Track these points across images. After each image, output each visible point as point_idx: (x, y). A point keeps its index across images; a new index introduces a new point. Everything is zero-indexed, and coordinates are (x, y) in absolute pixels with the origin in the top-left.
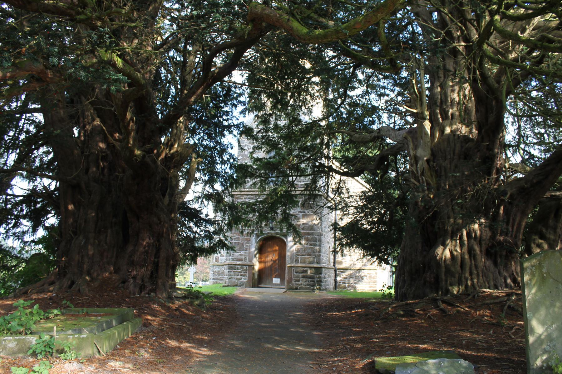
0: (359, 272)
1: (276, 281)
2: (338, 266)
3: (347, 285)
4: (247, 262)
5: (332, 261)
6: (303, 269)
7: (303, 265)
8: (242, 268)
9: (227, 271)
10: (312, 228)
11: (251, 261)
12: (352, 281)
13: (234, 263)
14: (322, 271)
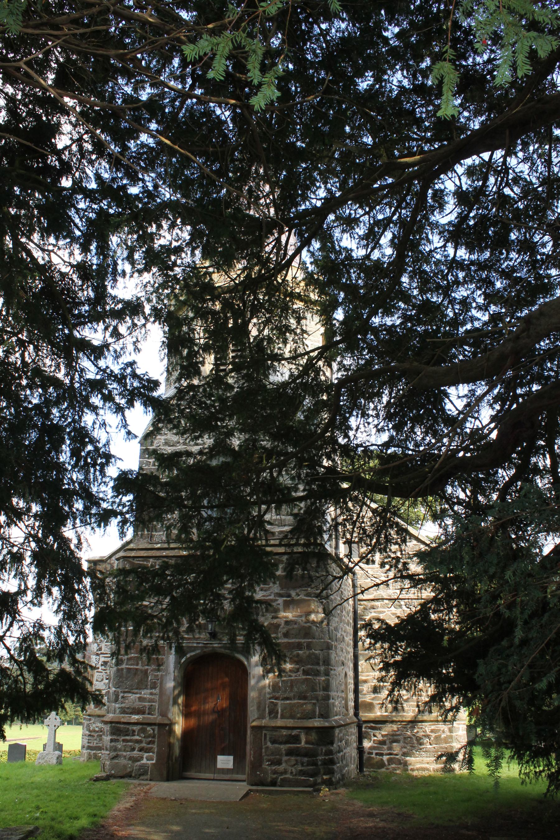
0: (413, 728)
1: (225, 761)
2: (365, 715)
3: (385, 758)
4: (156, 717)
5: (352, 704)
6: (289, 732)
7: (290, 723)
8: (143, 731)
9: (109, 738)
10: (306, 631)
11: (164, 714)
12: (397, 748)
13: (125, 718)
14: (333, 736)
